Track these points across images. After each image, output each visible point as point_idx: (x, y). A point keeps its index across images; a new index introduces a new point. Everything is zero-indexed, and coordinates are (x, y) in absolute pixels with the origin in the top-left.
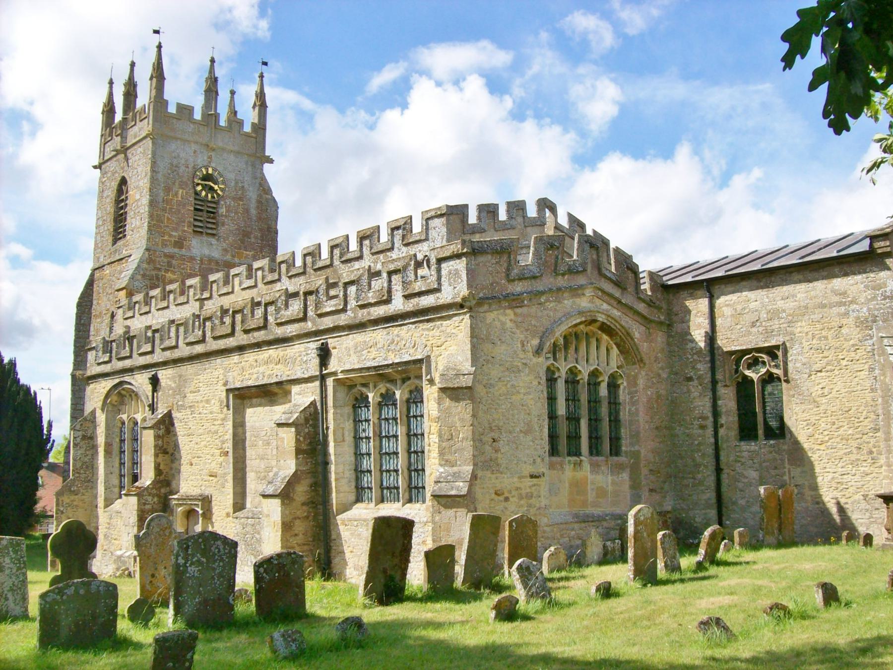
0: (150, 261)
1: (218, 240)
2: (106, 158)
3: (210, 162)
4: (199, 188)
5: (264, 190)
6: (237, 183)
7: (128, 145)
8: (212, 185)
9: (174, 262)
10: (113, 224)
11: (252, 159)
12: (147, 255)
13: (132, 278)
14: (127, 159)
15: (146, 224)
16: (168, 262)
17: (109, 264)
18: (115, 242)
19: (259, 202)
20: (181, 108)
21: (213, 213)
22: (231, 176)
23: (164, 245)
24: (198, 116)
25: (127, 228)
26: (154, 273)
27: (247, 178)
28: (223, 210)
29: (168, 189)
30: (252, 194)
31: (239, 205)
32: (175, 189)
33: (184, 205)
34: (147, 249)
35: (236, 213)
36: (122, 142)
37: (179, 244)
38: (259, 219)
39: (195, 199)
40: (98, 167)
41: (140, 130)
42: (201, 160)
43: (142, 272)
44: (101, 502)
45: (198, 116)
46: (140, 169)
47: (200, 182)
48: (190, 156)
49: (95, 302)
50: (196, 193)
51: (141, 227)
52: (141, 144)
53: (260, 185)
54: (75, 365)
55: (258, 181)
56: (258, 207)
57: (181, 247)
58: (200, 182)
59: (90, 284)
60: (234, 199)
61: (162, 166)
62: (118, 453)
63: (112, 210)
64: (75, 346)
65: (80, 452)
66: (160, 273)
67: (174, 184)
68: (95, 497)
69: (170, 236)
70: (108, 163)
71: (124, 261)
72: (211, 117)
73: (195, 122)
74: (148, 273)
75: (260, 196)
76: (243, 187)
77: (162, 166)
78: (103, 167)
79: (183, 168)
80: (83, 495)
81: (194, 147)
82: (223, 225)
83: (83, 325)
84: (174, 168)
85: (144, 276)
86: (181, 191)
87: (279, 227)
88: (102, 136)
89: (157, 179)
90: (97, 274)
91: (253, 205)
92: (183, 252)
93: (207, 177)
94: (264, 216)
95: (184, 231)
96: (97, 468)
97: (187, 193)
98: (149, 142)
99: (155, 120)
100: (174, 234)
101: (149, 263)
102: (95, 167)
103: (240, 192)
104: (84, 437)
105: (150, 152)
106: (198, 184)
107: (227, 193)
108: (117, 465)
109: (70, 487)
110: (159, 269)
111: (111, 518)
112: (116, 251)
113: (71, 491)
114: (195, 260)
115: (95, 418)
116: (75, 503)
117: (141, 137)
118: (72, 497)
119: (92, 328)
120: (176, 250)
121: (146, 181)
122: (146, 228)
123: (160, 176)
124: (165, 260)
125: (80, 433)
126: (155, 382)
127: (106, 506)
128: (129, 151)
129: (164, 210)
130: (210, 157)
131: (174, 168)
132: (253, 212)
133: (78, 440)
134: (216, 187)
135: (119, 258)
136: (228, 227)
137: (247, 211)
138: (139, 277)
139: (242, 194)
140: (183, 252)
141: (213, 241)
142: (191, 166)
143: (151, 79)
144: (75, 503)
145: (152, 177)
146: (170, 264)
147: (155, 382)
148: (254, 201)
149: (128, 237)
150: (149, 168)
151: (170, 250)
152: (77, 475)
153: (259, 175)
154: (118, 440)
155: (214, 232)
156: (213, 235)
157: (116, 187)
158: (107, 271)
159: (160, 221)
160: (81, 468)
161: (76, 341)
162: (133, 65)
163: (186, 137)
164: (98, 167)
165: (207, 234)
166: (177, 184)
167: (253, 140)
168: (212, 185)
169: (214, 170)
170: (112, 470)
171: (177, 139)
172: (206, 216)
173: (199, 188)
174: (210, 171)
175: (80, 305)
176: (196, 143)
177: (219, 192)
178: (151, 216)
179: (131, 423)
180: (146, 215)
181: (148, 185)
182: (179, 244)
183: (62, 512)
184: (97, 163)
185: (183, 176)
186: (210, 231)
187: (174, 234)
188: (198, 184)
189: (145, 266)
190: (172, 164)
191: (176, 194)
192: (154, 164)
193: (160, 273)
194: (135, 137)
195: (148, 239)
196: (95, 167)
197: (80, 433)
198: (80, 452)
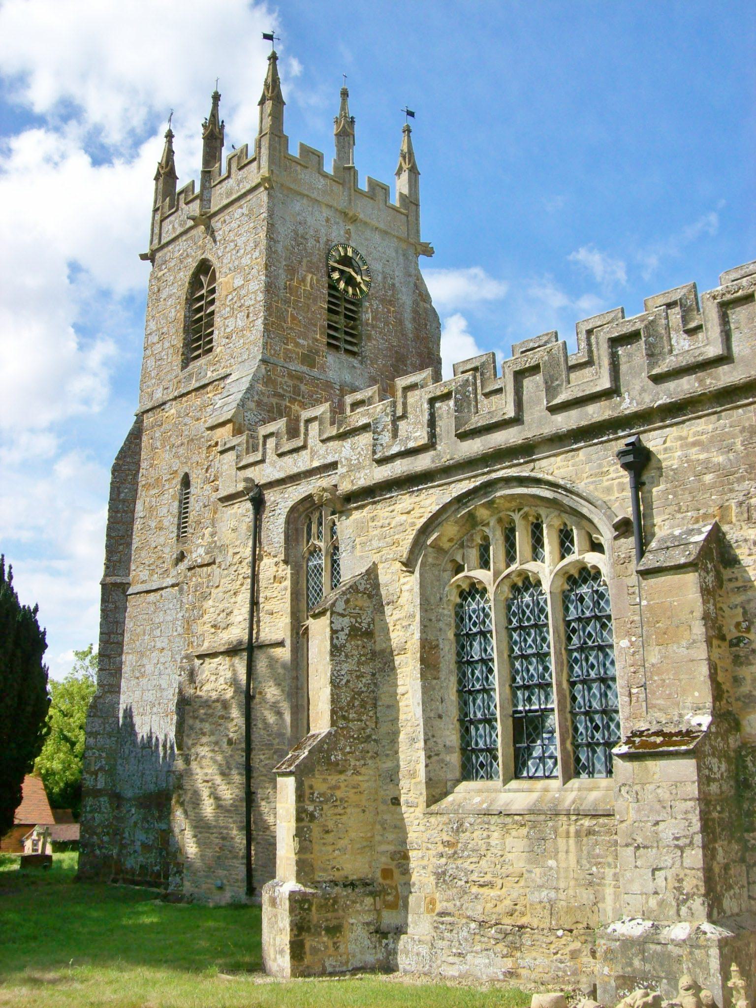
0: (268, 381)
1: (361, 363)
2: (163, 241)
3: (348, 239)
4: (336, 275)
5: (420, 295)
6: (385, 278)
7: (213, 209)
8: (353, 274)
9: (303, 387)
10: (182, 335)
11: (404, 246)
12: (263, 371)
13: (242, 404)
14: (211, 231)
15: (260, 322)
16: (295, 387)
17: (175, 398)
18: (185, 364)
19: (415, 311)
20: (306, 150)
21: (352, 317)
22: (376, 266)
23: (288, 358)
24: (329, 168)
25: (215, 336)
26: (274, 401)
27: (399, 273)
28: (367, 316)
29: (291, 271)
30: (406, 299)
31: (389, 311)
32: (302, 271)
33: (315, 300)
34: (263, 361)
35: (387, 323)
36: (202, 207)
37: (309, 359)
38: (417, 338)
39: (330, 295)
40: (149, 257)
41: (239, 183)
42: (337, 234)
43: (256, 398)
44: (412, 789)
45: (329, 168)
46: (240, 241)
47: (336, 265)
48: (322, 226)
49: (144, 465)
50: (333, 287)
51: (250, 327)
52: (243, 202)
53: (416, 285)
54: (107, 567)
55: (413, 280)
56: (414, 319)
57: (312, 365)
58: (336, 265)
59: (136, 435)
60: (382, 301)
61: (284, 231)
62: (453, 666)
63: (181, 316)
64: (108, 535)
65: (346, 667)
66: (283, 403)
67: (300, 262)
68: (392, 777)
69: (297, 345)
70: (170, 248)
71: (210, 388)
72: (346, 174)
73: (326, 176)
74: (265, 400)
75: (416, 303)
76: (393, 285)
77: (284, 231)
78: (158, 255)
79: (311, 243)
80: (358, 773)
81: (326, 213)
82: (369, 337)
83: (124, 501)
84: (299, 239)
85: (259, 403)
86: (309, 277)
87: (442, 355)
88: (156, 210)
89: (275, 252)
90: (148, 420)
91: (408, 315)
92: (315, 372)
93: (346, 261)
94: (423, 334)
95: (317, 340)
96: (393, 707)
97: (318, 281)
98: (262, 195)
99: (271, 161)
100: (301, 341)
101: (266, 384)
102: (144, 257)
103: (390, 293)
104: (355, 632)
105: (264, 209)
106: (334, 269)
107: (372, 291)
108: (452, 696)
109: (328, 752)
110: (282, 396)
111: (457, 831)
112: (191, 376)
113: (329, 763)
114: (332, 388)
115: (376, 586)
116: (339, 794)
117: (243, 191)
118: (333, 779)
119: (139, 507)
120: (305, 369)
121: (257, 254)
122: (261, 328)
123: (280, 248)
124: (291, 383)
125: (346, 621)
126: (639, 462)
127: (433, 799)
128: (213, 221)
129: (287, 302)
130: (348, 232)
131: (299, 239)
132: (409, 326)
133: (342, 636)
134: (359, 279)
135: (198, 385)
136: (375, 344)
137: (400, 322)
138: (252, 405)
139: (393, 295)
140: (315, 372)
141: (355, 362)
142: (323, 240)
143: (262, 103)
144: (339, 794)
145: (269, 248)
146: (296, 391)
147: (639, 462)
148: (408, 309)
149: (218, 350)
150: (263, 235)
151: (296, 366)
152: (341, 723)
153: (413, 272)
154: (451, 635)
155: (355, 349)
156: (353, 354)
157: (187, 279)
158: (172, 410)
159: (281, 318)
160: (351, 705)
161: (110, 528)
162: (216, 97)
163: (314, 195)
164: (149, 257)
165: (347, 351)
166: (304, 264)
167: (403, 217)
168: (353, 274)
169: (355, 252)
170: (441, 708)
171: (303, 195)
172: (344, 322)
173: (336, 275)
174: (350, 253)
175: (116, 470)
176: (330, 206)
177: (362, 286)
178: (268, 308)
179: (506, 588)
180: (260, 307)
181: (262, 261)
182: (309, 359)
183: (312, 817)
184: (147, 250)
185: (311, 254)
186: (349, 347)
187: (301, 341)
188: (334, 269)
189: (260, 387)
190: (296, 234)
191: (304, 280)
192: (271, 229)
193: (283, 403)
194: (228, 196)
195: (265, 345)
196: (144, 257)
197: (346, 621)
198: (346, 667)
